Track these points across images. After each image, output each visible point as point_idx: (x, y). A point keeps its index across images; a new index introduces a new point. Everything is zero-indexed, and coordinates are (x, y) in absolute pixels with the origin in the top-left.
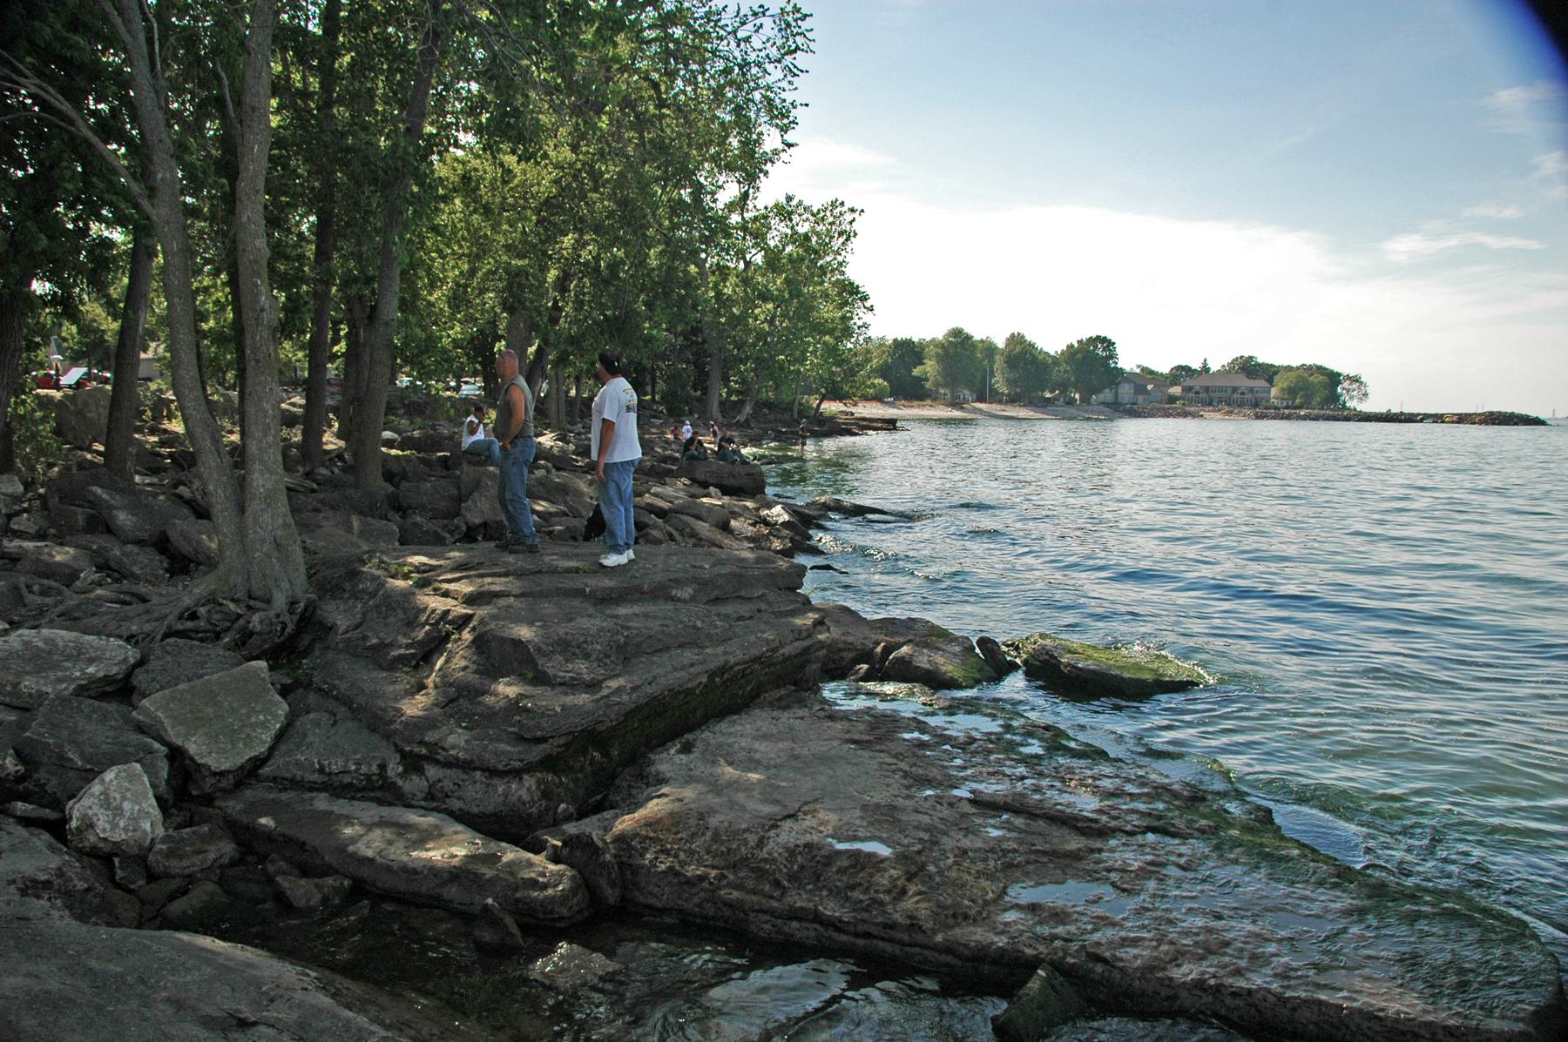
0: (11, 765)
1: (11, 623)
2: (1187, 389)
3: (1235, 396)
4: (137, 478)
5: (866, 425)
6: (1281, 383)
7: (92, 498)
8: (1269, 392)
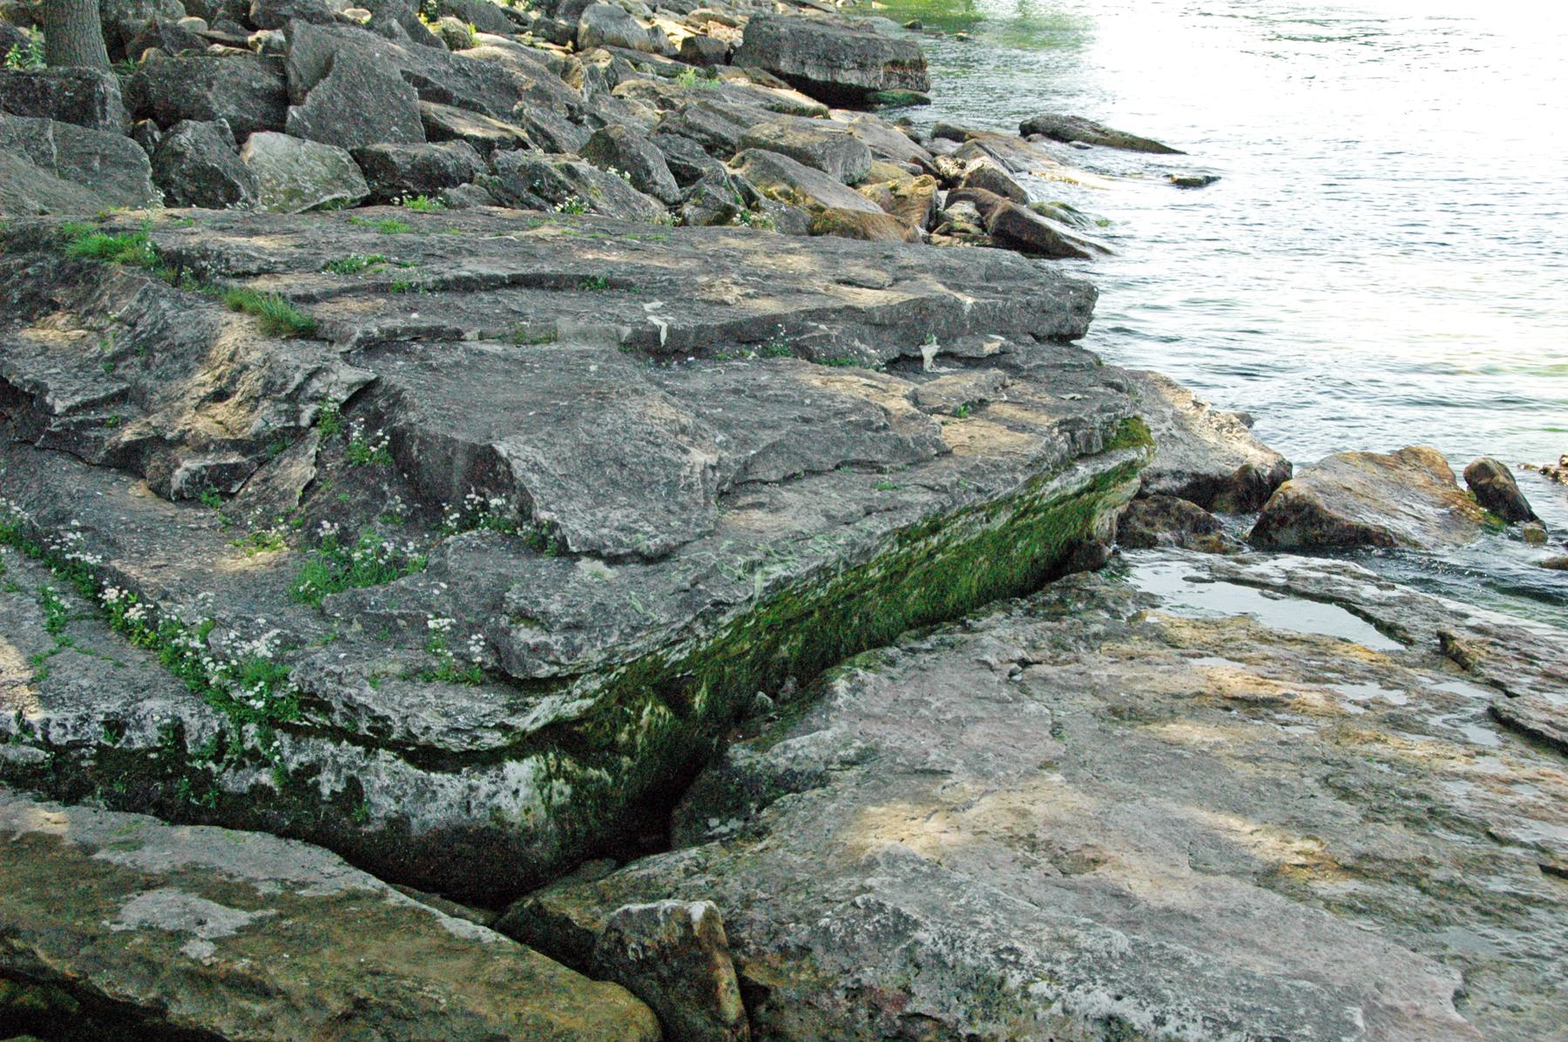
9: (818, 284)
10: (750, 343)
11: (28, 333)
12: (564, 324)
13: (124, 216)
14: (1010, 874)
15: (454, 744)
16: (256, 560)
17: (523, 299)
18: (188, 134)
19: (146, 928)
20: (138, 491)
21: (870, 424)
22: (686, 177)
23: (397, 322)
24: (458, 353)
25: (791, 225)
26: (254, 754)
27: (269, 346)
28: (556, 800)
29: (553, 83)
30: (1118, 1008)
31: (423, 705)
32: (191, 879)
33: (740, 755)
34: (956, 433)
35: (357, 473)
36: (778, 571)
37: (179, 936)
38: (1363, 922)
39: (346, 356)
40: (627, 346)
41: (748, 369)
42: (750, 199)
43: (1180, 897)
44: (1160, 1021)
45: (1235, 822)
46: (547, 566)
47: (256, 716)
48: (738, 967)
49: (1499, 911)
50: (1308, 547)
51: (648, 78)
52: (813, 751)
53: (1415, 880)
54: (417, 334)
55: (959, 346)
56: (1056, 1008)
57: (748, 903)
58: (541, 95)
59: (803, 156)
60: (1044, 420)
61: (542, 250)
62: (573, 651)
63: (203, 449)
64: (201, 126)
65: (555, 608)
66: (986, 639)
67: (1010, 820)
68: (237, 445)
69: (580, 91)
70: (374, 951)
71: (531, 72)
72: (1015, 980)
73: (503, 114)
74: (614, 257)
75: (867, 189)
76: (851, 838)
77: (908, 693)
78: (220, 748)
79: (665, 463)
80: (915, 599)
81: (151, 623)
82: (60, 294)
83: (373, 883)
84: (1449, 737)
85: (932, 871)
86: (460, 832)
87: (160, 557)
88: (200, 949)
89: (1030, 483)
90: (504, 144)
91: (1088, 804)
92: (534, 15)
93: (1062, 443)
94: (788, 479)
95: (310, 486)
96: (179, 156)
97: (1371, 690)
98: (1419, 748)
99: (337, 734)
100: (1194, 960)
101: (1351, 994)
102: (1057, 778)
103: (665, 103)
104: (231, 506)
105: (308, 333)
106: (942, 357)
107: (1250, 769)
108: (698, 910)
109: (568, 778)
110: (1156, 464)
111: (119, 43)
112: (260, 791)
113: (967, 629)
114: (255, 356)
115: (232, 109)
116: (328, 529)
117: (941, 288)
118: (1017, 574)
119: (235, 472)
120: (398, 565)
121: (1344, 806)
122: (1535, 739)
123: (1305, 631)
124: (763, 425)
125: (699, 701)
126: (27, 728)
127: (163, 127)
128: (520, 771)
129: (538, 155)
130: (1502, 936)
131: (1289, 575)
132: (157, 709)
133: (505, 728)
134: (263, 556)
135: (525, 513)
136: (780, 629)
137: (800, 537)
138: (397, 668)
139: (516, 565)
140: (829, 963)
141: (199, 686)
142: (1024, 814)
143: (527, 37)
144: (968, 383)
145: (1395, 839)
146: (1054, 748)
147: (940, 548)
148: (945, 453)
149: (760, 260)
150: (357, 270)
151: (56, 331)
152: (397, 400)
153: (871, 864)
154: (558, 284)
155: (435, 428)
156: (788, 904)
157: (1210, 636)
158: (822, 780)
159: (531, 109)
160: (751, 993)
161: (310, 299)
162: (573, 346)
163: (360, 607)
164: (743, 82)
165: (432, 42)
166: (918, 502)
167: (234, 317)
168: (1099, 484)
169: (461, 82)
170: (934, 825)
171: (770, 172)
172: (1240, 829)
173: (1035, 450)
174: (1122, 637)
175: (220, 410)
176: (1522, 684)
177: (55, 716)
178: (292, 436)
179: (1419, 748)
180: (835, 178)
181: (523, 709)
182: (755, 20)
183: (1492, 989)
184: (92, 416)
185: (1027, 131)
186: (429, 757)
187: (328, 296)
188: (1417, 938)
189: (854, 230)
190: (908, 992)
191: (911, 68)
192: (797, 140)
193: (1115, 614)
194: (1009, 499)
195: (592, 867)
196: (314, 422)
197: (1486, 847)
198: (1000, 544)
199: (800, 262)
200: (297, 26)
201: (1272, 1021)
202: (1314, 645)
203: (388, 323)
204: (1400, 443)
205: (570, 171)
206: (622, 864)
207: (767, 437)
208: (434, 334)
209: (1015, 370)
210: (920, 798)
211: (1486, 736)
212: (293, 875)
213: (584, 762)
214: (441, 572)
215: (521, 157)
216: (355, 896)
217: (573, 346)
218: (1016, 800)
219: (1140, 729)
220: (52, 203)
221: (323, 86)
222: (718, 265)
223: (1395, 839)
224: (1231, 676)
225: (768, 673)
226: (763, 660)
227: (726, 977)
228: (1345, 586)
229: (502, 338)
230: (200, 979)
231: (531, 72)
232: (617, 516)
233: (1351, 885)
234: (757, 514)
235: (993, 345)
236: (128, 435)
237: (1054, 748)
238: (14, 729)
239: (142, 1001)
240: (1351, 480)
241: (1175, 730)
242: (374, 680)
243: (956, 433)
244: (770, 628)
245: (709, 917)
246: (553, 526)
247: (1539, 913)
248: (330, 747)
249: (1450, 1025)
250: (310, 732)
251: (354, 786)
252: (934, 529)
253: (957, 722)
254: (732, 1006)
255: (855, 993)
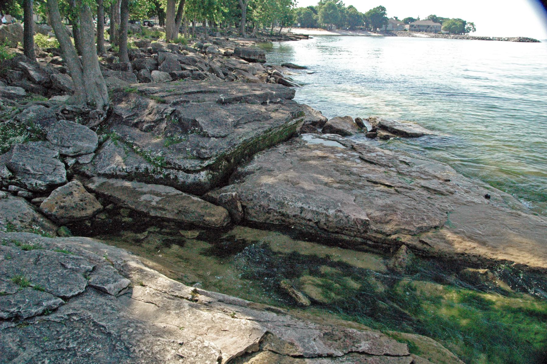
0: (6, 173)
1: (64, 298)
2: (411, 26)
3: (429, 29)
4: (37, 59)
5: (297, 37)
6: (445, 25)
7: (20, 66)
8: (441, 28)
9: (249, 91)
10: (238, 101)
11: (119, 105)
12: (206, 99)
13: (133, 85)
14: (285, 186)
15: (192, 169)
16: (157, 141)
17: (201, 96)
18: (142, 72)
19: (144, 200)
20: (138, 130)
21: (258, 114)
22: (225, 74)
23: (179, 100)
24: (189, 105)
25: (243, 81)
26: (159, 172)
27: (158, 105)
28: (210, 178)
29: (202, 60)
30: (302, 206)
31: (187, 163)
32: (152, 193)
33: (240, 169)
34: (273, 115)
35: (173, 125)
36: (244, 138)
37: (150, 201)
38: (341, 190)
39: (170, 106)
40: (217, 102)
41: (237, 105)
42: (236, 78)
43: (312, 188)
44: (309, 207)
45: (320, 176)
46: (206, 139)
47: (159, 166)
48: (241, 203)
49: (361, 187)
50: (331, 133)
51: (218, 59)
52: (252, 168)
53: (348, 183)
54: (182, 101)
55: (273, 100)
56: (293, 206)
57: (242, 192)
58: (201, 62)
59: (245, 71)
60: (288, 112)
61: (202, 87)
62: (211, 153)
63: (148, 123)
64: (144, 70)
65: (207, 146)
66: (279, 149)
67: (285, 177)
68: (153, 122)
69: (207, 61)
70: (181, 203)
71: (199, 58)
72: (286, 202)
73: (194, 66)
74: (214, 87)
75: (256, 76)
76: (259, 181)
77: (267, 158)
78: (154, 171)
79: (225, 121)
80: (267, 143)
81: (141, 151)
82: (124, 99)
83: (181, 192)
84: (353, 161)
85: (271, 186)
86: (194, 183)
87: (142, 141)
88: (154, 203)
89: (286, 123)
90: (194, 70)
91: (297, 174)
92: (199, 49)
93: (291, 116)
94: (246, 123)
95: (165, 128)
96: (141, 75)
97: (341, 154)
98: (348, 163)
99: (173, 168)
100: (314, 198)
101: (338, 201)
102: (292, 170)
103: (221, 63)
104: (153, 132)
105: (164, 102)
106: (270, 102)
107: (323, 168)
108: (234, 194)
109: (211, 174)
110: (306, 119)
111: (131, 58)
112: (161, 178)
113: (276, 147)
114: (155, 107)
115: (149, 67)
116: (169, 135)
117: (269, 91)
118: (284, 138)
119: (153, 126)
120: (181, 140)
121: (337, 173)
122: (366, 161)
123: (331, 145)
124: (241, 114)
125: (232, 161)
126: (123, 169)
127: (138, 71)
128: (203, 173)
129: (200, 72)
130: (361, 191)
131: (328, 137)
132: (143, 166)
133: (200, 166)
134: (159, 140)
135: (201, 130)
136: (245, 149)
137: (248, 133)
138: (182, 157)
139: (200, 139)
140: (256, 201)
141: (150, 161)
142: (287, 176)
143: (197, 53)
144: (275, 106)
145: (345, 178)
146: (291, 166)
147: (271, 134)
148: (271, 118)
149: (239, 87)
150: (171, 92)
151: (123, 105)
152: (179, 113)
153: (262, 185)
154: (205, 92)
155: (186, 117)
156: (248, 192)
157: (316, 147)
158: (253, 173)
159: (199, 64)
160: (243, 207)
161: (164, 97)
162: (208, 102)
163: (175, 147)
164: (234, 59)
165: (182, 54)
166: (267, 126)
167: (151, 100)
168: (297, 123)
169: (187, 61)
170: (272, 179)
171: (239, 73)
172: (322, 177)
173: (286, 117)
174: (302, 148)
175: (150, 116)
176: (364, 152)
177: (127, 167)
178: (161, 120)
179: (348, 163)
180: (251, 74)
181: (203, 163)
182: (236, 48)
183: (360, 199)
184: (130, 118)
185: (283, 66)
186: (188, 171)
187: (166, 96)
188: (349, 192)
189: (255, 82)
190: (269, 205)
191: (262, 56)
192: (244, 68)
193: (300, 144)
194: (282, 126)
195: (216, 188)
196: (166, 117)
197: (359, 178)
198: (281, 133)
199: (246, 87)
200: (159, 53)
201: (327, 206)
202: (333, 148)
203: (177, 100)
204: (346, 115)
205: (206, 74)
206: (221, 187)
207: (242, 116)
208: (185, 101)
209: (282, 104)
210: (270, 175)
211: (359, 161)
212: (167, 191)
213: (213, 172)
214: (188, 141)
215: (197, 72)
216: (178, 194)
217: (208, 102)
218: (285, 174)
219: (305, 162)
220: (122, 84)
221: (164, 62)
222: (232, 88)
223: (345, 178)
224: (319, 153)
225: (243, 156)
226: (242, 154)
227: (239, 205)
228: (337, 138)
229: (196, 102)
230: (154, 208)
231: (199, 58)
232: (217, 130)
233: (339, 185)
234: (240, 129)
235: (279, 100)
236: (135, 121)
237: (291, 166)
238: (121, 170)
239: (145, 211)
240: (337, 121)
241: (311, 162)
242: (178, 159)
243: (273, 115)
244: (243, 148)
245: (236, 195)
246: (206, 132)
247: (366, 187)
248: (172, 170)
249: (353, 205)
250: (169, 168)
251: (176, 177)
252: (270, 131)
253: (275, 162)
254: (240, 209)
255: (260, 206)
